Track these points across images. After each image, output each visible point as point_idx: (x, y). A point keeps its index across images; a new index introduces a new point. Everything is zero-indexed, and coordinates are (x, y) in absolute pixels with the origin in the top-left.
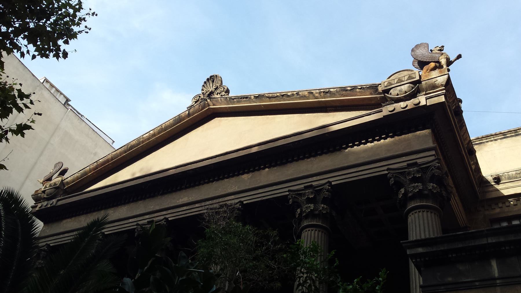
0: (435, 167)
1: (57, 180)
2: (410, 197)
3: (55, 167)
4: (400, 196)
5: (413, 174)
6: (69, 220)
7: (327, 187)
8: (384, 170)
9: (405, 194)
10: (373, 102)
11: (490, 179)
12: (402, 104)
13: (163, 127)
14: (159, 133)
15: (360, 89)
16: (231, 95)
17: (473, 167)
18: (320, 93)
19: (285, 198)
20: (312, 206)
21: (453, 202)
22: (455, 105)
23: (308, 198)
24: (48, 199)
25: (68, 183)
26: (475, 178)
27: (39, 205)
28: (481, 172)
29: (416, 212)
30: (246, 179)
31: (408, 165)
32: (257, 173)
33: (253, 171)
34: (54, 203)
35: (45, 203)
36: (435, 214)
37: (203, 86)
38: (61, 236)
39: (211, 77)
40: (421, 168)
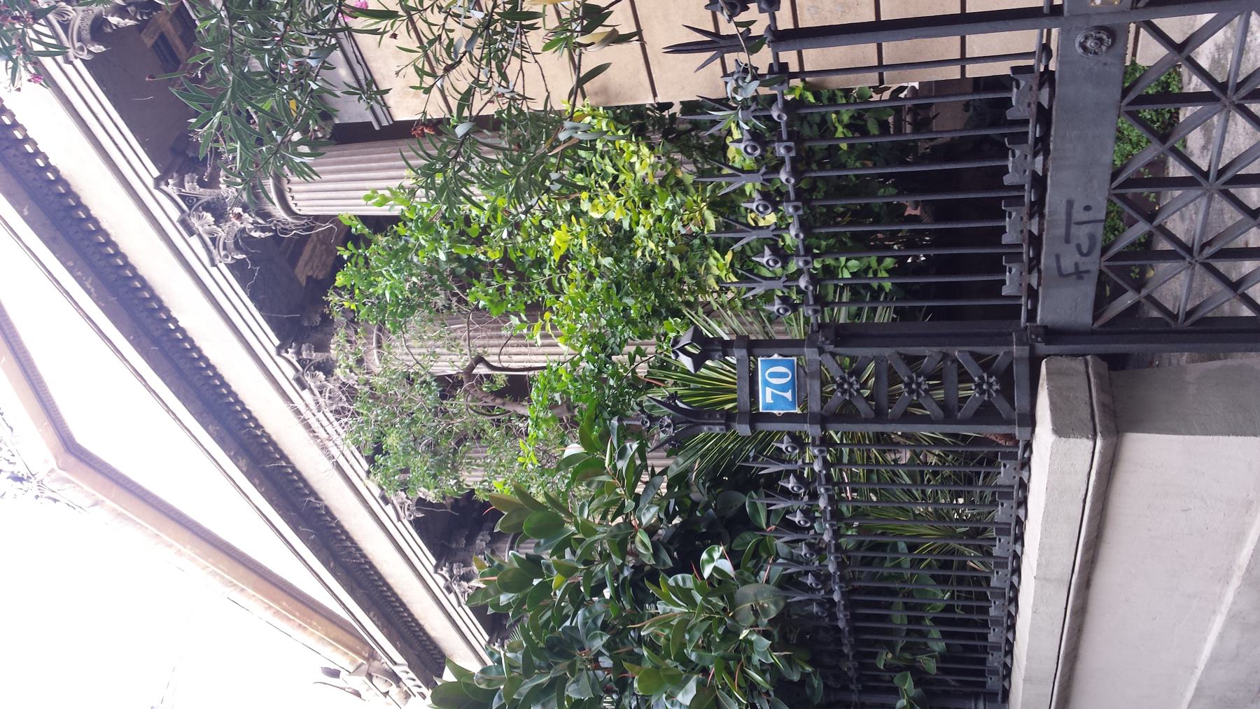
7: (445, 571)
23: (217, 223)
33: (191, 341)
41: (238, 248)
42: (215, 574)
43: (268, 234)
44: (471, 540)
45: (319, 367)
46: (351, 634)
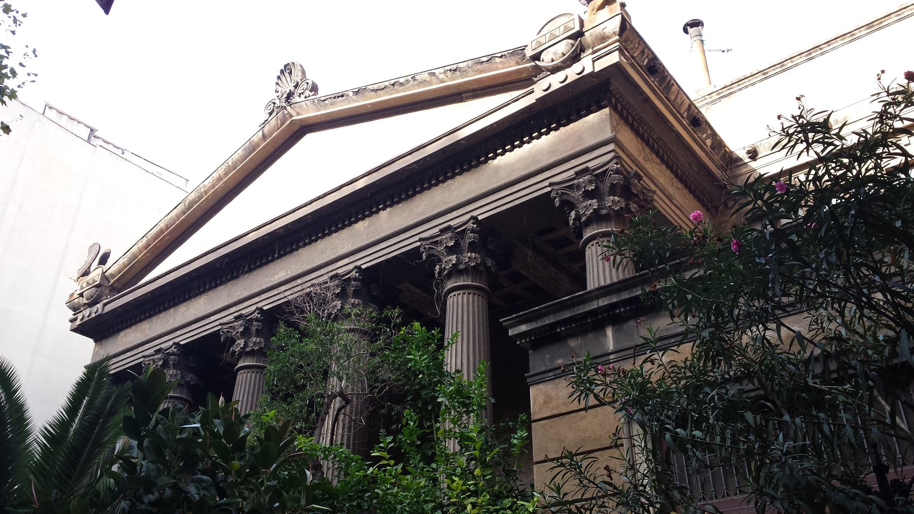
1: (96, 275)
3: (90, 252)
4: (571, 222)
6: (128, 331)
7: (470, 225)
9: (578, 217)
10: (524, 75)
11: (742, 154)
12: (560, 75)
13: (230, 163)
14: (226, 174)
15: (501, 57)
16: (322, 93)
18: (445, 72)
19: (416, 252)
20: (594, 203)
22: (647, 57)
23: (447, 247)
24: (91, 305)
25: (112, 276)
27: (80, 316)
28: (725, 146)
30: (362, 229)
31: (577, 173)
32: (374, 218)
33: (369, 216)
34: (100, 310)
35: (87, 312)
37: (277, 84)
38: (122, 357)
39: (286, 66)
40: (596, 176)
41: (227, 339)
42: (200, 197)
43: (437, 276)
44: (192, 370)
45: (344, 290)
46: (125, 285)
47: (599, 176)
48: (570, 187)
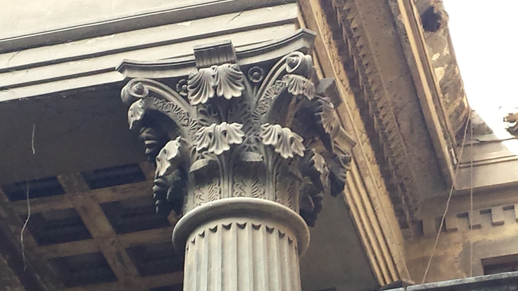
0: (292, 65)
2: (197, 173)
4: (163, 167)
5: (215, 88)
8: (112, 70)
9: (181, 163)
17: (439, 73)
21: (353, 193)
26: (438, 108)
29: (215, 230)
31: (200, 53)
36: (281, 236)
40: (245, 69)
47: (256, 74)
48: (171, 82)
